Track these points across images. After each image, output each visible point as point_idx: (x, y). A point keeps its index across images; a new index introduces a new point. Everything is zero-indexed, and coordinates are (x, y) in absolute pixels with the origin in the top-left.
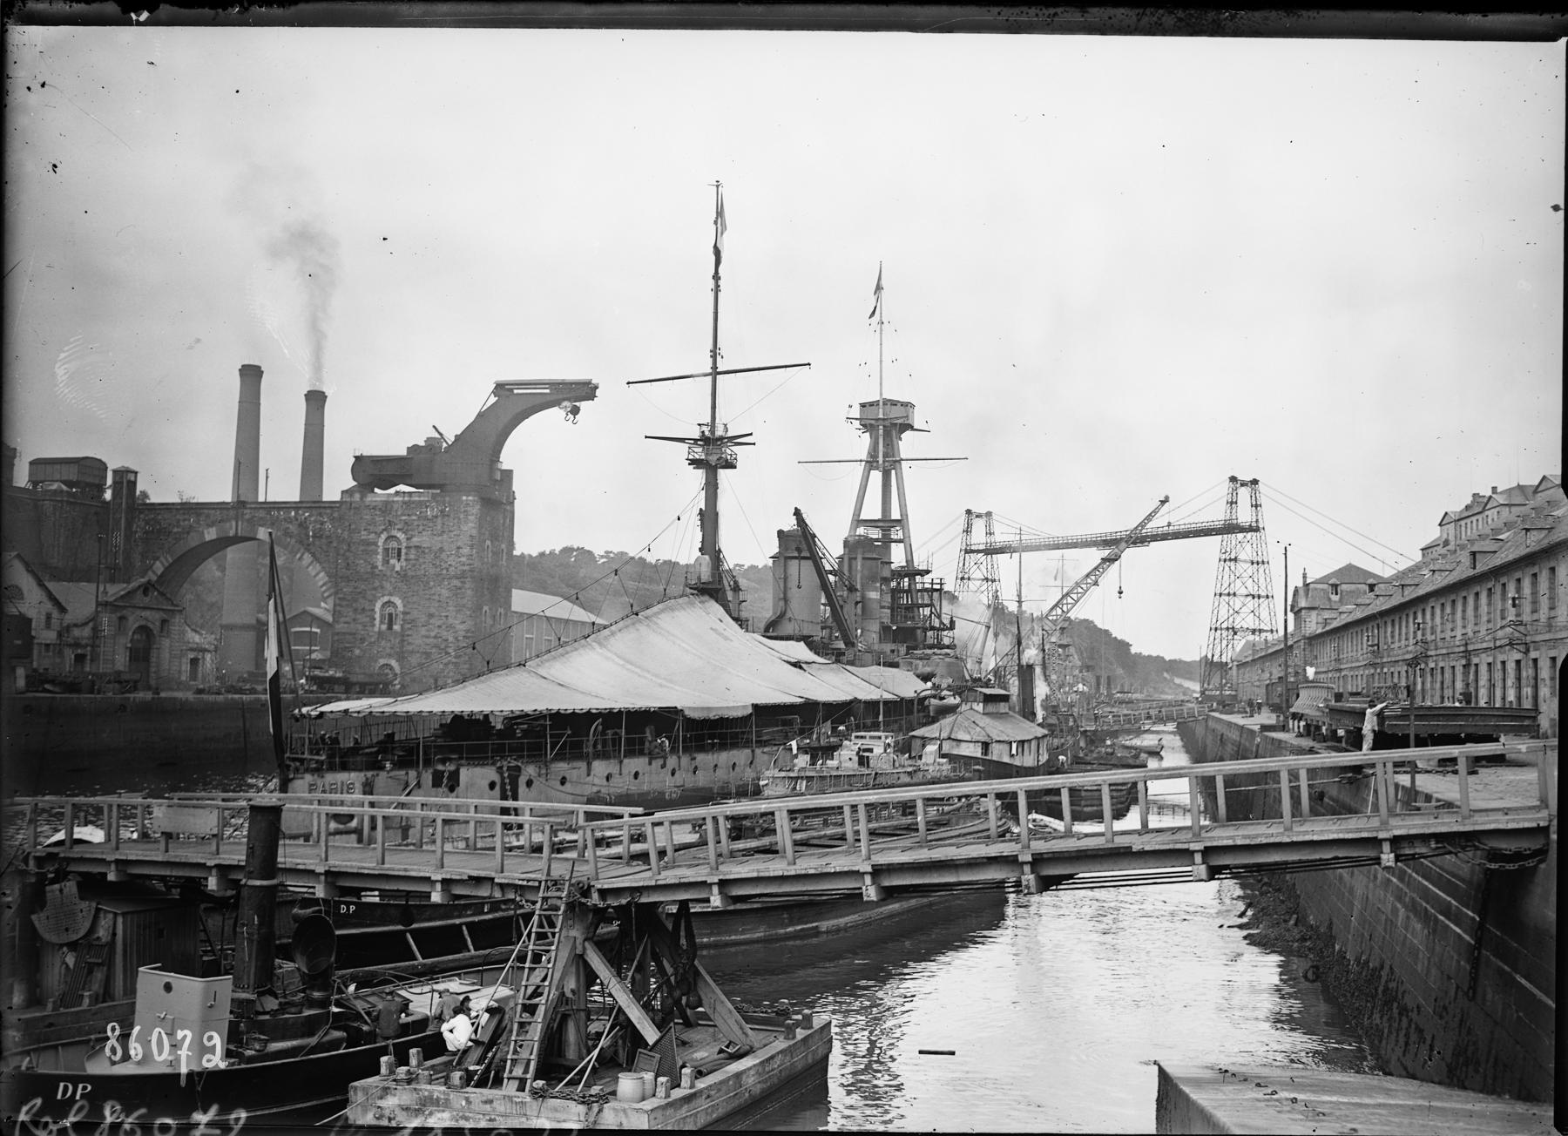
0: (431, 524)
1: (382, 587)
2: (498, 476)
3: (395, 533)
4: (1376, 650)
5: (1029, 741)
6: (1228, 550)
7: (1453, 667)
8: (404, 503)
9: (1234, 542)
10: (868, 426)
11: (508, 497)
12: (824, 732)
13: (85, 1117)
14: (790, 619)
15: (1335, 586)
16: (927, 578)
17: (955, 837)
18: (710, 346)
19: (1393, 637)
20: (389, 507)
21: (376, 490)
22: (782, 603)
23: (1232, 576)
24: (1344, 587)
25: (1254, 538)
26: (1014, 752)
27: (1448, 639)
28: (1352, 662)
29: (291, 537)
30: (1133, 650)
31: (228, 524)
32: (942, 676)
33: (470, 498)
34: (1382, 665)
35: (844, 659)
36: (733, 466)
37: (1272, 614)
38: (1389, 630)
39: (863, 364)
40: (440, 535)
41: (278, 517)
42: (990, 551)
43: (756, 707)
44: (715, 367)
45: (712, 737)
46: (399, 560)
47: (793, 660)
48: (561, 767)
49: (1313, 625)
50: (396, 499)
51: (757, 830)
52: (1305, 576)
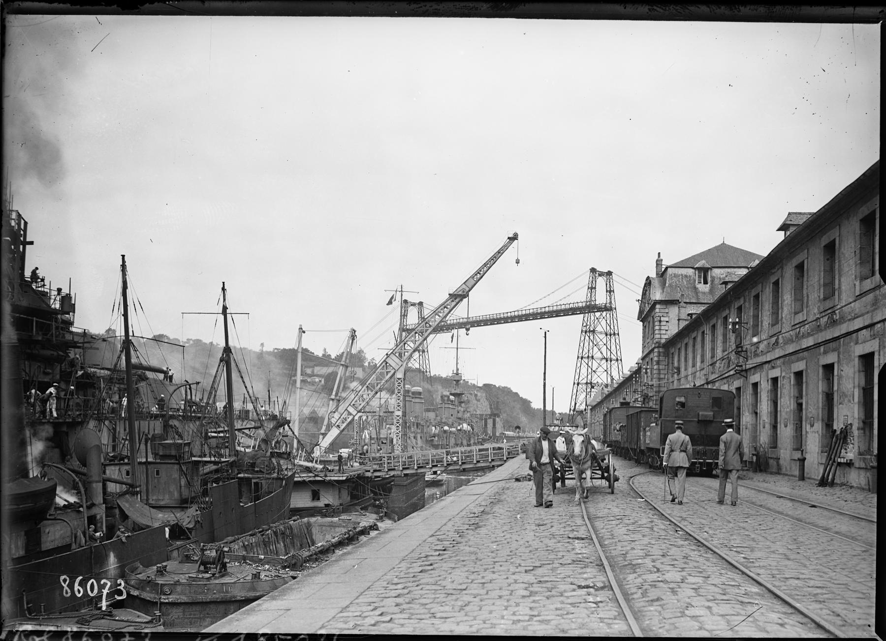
9: (592, 318)
24: (717, 272)
25: (608, 315)
30: (33, 260)
52: (659, 263)
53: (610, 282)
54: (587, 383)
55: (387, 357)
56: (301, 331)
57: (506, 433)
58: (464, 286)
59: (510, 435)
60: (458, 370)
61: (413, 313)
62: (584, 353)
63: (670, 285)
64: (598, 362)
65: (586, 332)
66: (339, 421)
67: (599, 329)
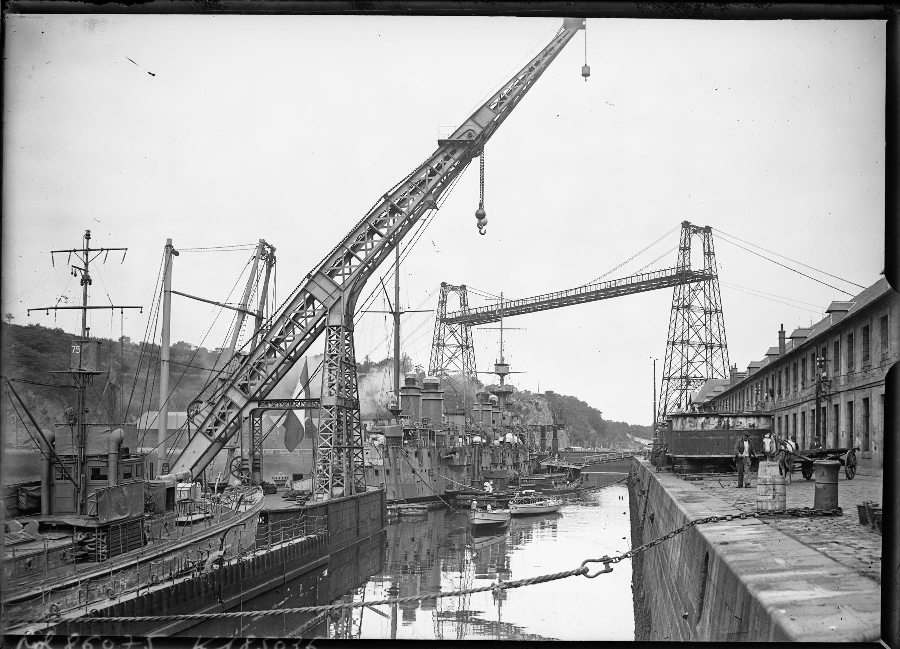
25: (707, 286)
53: (708, 241)
54: (681, 377)
55: (309, 282)
56: (170, 251)
57: (573, 447)
58: (471, 126)
59: (578, 450)
60: (503, 359)
61: (454, 300)
62: (676, 337)
64: (696, 348)
65: (678, 309)
66: (210, 422)
67: (695, 303)
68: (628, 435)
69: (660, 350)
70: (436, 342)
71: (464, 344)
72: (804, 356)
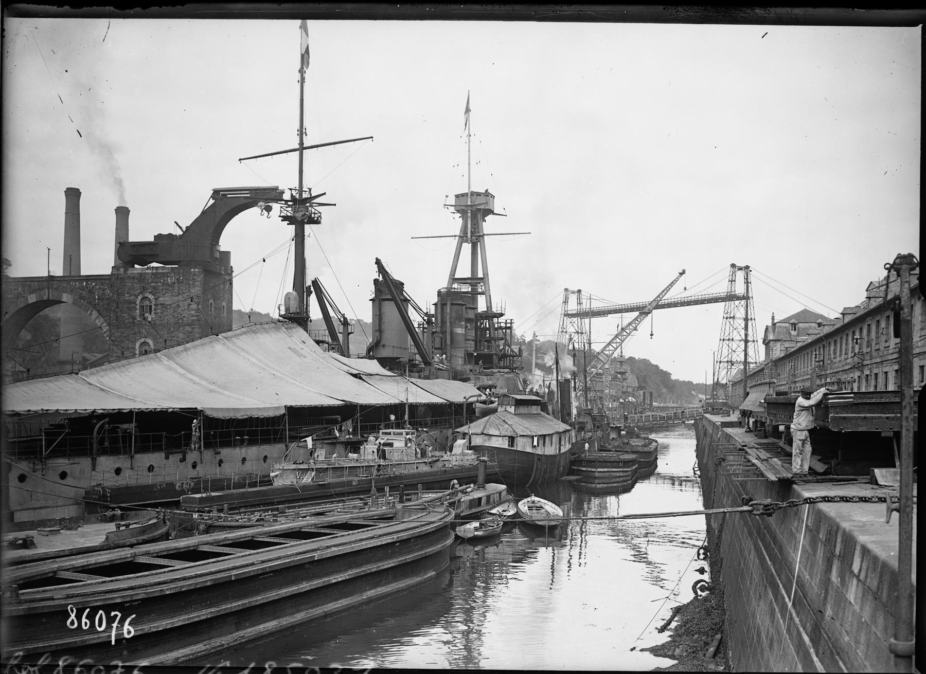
0: (171, 289)
1: (140, 333)
2: (218, 255)
3: (147, 295)
4: (822, 365)
5: (551, 435)
6: (729, 311)
7: (886, 373)
8: (153, 274)
9: (733, 306)
10: (461, 210)
11: (226, 270)
12: (345, 431)
13: (49, 662)
14: (384, 346)
15: (794, 325)
16: (502, 319)
17: (366, 539)
18: (298, 126)
19: (835, 353)
20: (143, 277)
21: (136, 266)
22: (377, 334)
23: (731, 328)
24: (800, 325)
26: (535, 443)
27: (882, 349)
28: (804, 376)
29: (84, 300)
30: (673, 377)
31: (43, 291)
32: (501, 388)
33: (197, 270)
34: (826, 376)
35: (422, 375)
36: (317, 222)
37: (757, 352)
38: (832, 348)
39: (456, 166)
40: (177, 296)
41: (74, 286)
42: (582, 315)
43: (290, 410)
44: (301, 143)
45: (241, 434)
46: (150, 314)
47: (356, 372)
48: (62, 463)
49: (778, 352)
50: (147, 271)
51: (202, 527)
52: (773, 318)
61: (573, 299)
62: (725, 336)
63: (778, 332)
68: (693, 392)
69: (715, 344)
70: (561, 330)
71: (580, 331)
72: (847, 332)
